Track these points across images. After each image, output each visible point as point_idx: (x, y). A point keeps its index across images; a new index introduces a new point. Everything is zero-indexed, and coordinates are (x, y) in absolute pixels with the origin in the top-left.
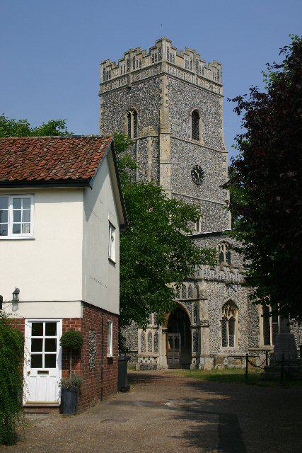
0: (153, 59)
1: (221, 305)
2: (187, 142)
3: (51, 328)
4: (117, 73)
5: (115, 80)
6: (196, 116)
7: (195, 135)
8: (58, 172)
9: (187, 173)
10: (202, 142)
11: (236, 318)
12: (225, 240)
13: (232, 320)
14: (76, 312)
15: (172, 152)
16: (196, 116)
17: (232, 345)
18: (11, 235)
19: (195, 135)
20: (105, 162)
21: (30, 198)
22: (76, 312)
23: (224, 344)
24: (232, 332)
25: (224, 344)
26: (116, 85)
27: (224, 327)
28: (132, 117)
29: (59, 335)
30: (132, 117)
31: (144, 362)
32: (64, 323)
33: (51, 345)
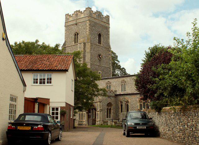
0: (84, 15)
1: (106, 104)
2: (96, 45)
3: (57, 109)
4: (71, 19)
5: (70, 21)
6: (100, 35)
7: (100, 42)
8: (59, 67)
9: (74, 129)
10: (102, 45)
11: (112, 108)
12: (109, 81)
13: (110, 109)
14: (64, 105)
15: (91, 48)
16: (100, 35)
17: (110, 117)
18: (46, 84)
19: (100, 42)
20: (71, 64)
21: (51, 74)
22: (64, 105)
23: (107, 117)
24: (110, 113)
25: (107, 117)
26: (71, 23)
27: (107, 111)
28: (77, 35)
29: (59, 111)
30: (77, 35)
31: (80, 123)
32: (34, 111)
33: (57, 114)
